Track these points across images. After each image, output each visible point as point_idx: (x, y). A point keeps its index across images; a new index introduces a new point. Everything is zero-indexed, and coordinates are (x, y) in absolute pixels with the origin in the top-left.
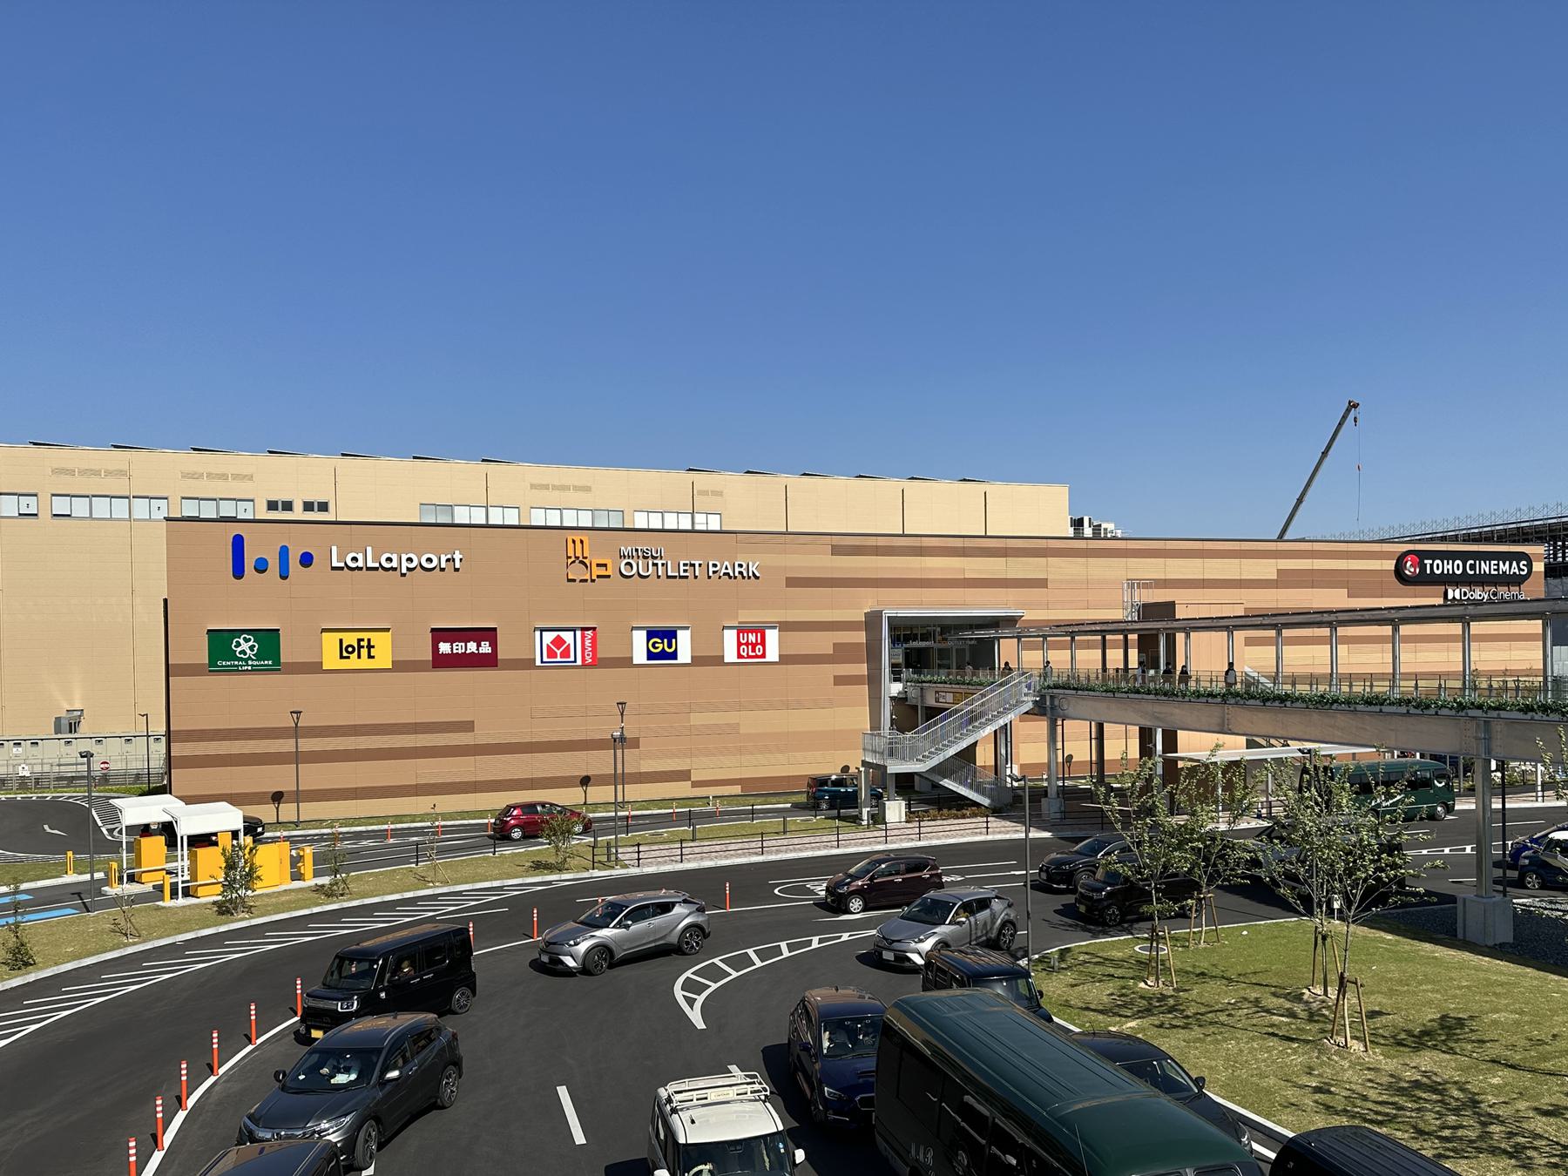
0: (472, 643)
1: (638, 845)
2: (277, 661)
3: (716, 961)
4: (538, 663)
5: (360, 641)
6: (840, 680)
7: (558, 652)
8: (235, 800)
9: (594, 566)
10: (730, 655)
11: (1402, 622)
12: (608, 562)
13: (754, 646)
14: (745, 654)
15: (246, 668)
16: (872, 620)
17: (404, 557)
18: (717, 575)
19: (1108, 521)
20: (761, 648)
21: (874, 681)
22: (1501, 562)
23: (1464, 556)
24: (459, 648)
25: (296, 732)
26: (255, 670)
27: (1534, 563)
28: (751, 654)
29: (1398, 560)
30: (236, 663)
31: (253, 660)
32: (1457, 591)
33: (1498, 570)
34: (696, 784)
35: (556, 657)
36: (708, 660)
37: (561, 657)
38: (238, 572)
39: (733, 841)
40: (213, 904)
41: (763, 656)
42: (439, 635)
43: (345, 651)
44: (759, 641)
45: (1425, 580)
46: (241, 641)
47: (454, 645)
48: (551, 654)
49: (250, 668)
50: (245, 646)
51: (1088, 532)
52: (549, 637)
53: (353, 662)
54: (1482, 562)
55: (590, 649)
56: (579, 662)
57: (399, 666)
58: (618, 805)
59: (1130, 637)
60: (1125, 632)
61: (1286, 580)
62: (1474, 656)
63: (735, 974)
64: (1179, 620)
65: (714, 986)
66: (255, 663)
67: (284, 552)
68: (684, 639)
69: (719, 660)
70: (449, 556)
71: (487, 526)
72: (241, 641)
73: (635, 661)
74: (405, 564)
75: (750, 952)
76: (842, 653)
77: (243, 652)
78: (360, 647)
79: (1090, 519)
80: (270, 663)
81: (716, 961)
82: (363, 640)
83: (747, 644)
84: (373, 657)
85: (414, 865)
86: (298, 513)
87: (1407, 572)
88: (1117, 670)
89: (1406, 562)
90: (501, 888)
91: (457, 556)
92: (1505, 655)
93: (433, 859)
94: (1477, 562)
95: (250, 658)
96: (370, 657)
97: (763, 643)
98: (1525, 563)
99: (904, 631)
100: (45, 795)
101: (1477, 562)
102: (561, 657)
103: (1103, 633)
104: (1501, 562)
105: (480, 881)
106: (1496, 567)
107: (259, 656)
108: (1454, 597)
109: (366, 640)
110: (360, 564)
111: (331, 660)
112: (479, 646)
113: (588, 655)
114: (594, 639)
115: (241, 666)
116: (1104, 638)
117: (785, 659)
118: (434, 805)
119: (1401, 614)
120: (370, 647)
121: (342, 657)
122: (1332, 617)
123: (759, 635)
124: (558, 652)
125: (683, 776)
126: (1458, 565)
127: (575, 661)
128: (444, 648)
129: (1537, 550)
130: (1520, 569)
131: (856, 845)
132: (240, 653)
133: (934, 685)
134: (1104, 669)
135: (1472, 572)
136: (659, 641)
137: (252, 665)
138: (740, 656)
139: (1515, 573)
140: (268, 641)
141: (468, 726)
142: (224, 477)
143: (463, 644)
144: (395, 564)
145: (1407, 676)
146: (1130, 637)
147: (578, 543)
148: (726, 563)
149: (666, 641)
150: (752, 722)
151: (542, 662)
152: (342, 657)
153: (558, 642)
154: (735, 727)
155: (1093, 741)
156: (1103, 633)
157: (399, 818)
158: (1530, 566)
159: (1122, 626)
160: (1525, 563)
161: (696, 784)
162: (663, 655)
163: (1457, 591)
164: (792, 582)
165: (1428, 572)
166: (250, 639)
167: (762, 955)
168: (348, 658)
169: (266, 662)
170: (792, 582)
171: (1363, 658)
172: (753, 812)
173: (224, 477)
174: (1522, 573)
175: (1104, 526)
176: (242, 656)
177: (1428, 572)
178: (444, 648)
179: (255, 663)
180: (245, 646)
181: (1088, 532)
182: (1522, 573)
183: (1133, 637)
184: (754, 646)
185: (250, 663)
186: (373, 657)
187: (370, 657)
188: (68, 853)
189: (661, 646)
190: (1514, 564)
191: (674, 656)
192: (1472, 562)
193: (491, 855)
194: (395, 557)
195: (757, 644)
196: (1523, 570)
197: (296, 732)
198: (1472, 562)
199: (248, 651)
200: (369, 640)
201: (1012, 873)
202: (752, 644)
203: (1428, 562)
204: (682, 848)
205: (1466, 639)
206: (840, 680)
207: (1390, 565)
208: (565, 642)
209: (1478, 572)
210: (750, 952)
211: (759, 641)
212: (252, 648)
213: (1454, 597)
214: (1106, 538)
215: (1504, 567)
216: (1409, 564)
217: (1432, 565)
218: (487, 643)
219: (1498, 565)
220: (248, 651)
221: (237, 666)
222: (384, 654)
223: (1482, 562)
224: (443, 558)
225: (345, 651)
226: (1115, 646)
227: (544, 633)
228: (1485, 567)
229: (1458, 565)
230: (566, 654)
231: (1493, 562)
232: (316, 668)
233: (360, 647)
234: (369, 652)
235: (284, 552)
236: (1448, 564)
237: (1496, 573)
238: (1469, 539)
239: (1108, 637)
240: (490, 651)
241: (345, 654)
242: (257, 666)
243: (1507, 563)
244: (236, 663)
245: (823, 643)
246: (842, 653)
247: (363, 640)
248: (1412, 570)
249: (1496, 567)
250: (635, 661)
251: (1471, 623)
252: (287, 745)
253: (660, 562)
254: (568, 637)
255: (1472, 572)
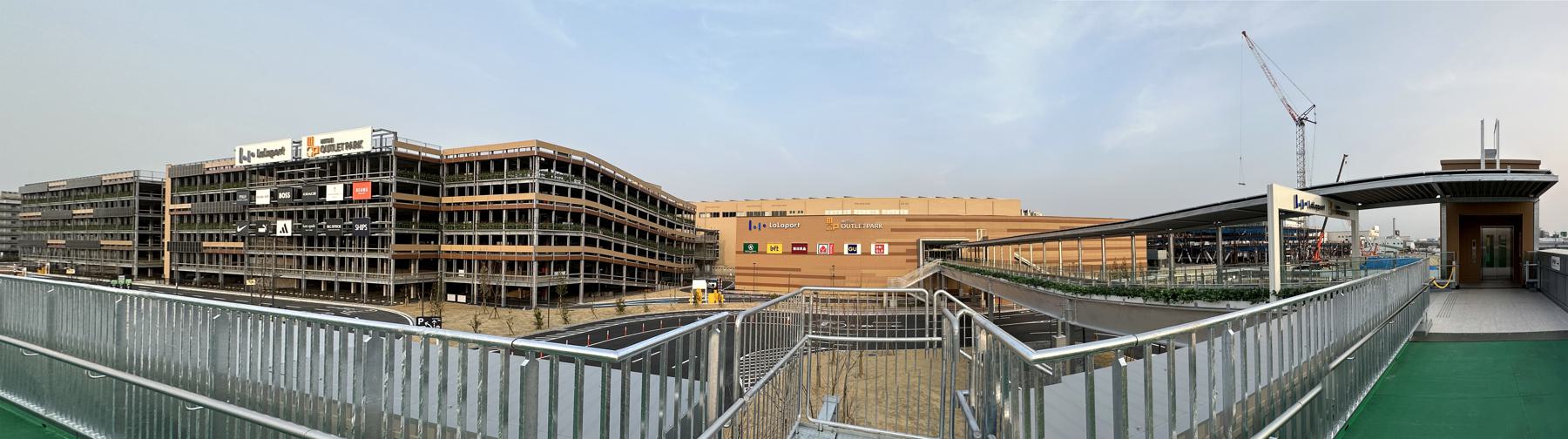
6: (908, 261)
10: (873, 252)
16: (918, 241)
24: (798, 249)
25: (754, 269)
36: (866, 253)
38: (750, 229)
42: (794, 245)
43: (772, 249)
51: (1029, 214)
52: (821, 246)
53: (774, 252)
57: (784, 253)
64: (258, 206)
69: (869, 254)
76: (909, 252)
86: (796, 214)
92: (1093, 254)
99: (928, 245)
111: (769, 251)
117: (890, 254)
128: (795, 249)
140: (756, 246)
142: (780, 206)
153: (823, 248)
164: (893, 230)
170: (893, 230)
171: (1088, 254)
173: (780, 206)
178: (795, 249)
180: (751, 247)
181: (1029, 214)
191: (856, 252)
197: (754, 269)
206: (908, 261)
222: (780, 251)
225: (772, 249)
232: (765, 253)
245: (902, 249)
246: (909, 252)
252: (752, 272)
254: (826, 246)
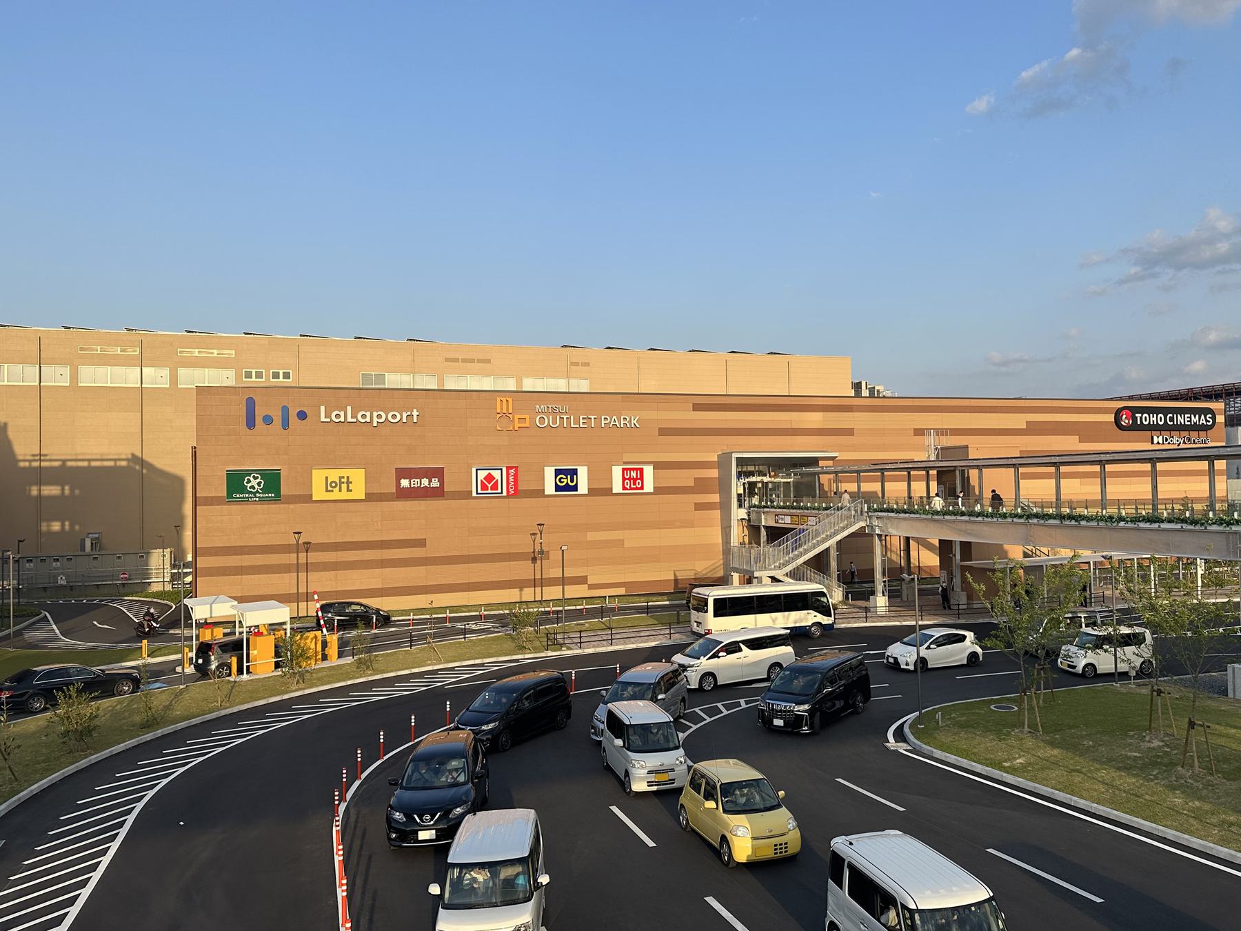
0: (425, 479)
1: (580, 632)
2: (278, 494)
3: (697, 710)
4: (474, 494)
5: (341, 478)
7: (489, 486)
8: (283, 599)
9: (516, 420)
10: (617, 487)
11: (1159, 460)
12: (527, 417)
13: (635, 480)
14: (628, 487)
15: (255, 499)
17: (375, 414)
18: (608, 425)
19: (878, 385)
20: (629, 482)
21: (725, 507)
22: (1192, 416)
23: (1165, 411)
24: (415, 483)
26: (261, 500)
27: (1217, 416)
28: (632, 486)
29: (1116, 414)
30: (247, 495)
31: (260, 493)
32: (1161, 437)
33: (1190, 421)
34: (591, 587)
35: (487, 490)
36: (600, 491)
37: (491, 490)
38: (251, 423)
39: (642, 629)
40: (562, 645)
41: (642, 488)
42: (402, 473)
44: (639, 477)
45: (1136, 427)
46: (251, 479)
47: (412, 481)
48: (484, 487)
49: (257, 499)
50: (254, 483)
54: (1179, 416)
55: (513, 483)
56: (505, 493)
57: (370, 497)
58: (564, 601)
59: (931, 472)
60: (927, 469)
61: (1033, 429)
62: (1109, 488)
63: (709, 720)
65: (695, 727)
66: (261, 495)
67: (285, 410)
68: (583, 473)
69: (608, 491)
70: (409, 413)
71: (789, 396)
72: (251, 479)
73: (547, 493)
74: (375, 420)
75: (719, 705)
77: (253, 487)
78: (341, 483)
79: (866, 383)
80: (273, 495)
81: (697, 710)
82: (343, 477)
83: (630, 479)
84: (351, 491)
85: (409, 648)
87: (1123, 423)
88: (921, 498)
89: (1122, 416)
90: (482, 665)
91: (415, 413)
93: (430, 643)
94: (1175, 415)
95: (257, 492)
96: (349, 490)
97: (642, 478)
98: (1211, 416)
100: (81, 599)
101: (1175, 415)
102: (491, 490)
103: (1056, 465)
104: (1192, 416)
105: (451, 662)
106: (1189, 419)
107: (265, 490)
108: (1158, 437)
109: (346, 477)
110: (342, 419)
111: (319, 493)
112: (430, 481)
113: (512, 488)
114: (516, 476)
115: (251, 498)
116: (909, 473)
117: (658, 490)
118: (432, 602)
119: (1108, 457)
120: (348, 483)
121: (327, 491)
122: (1057, 460)
123: (639, 472)
124: (489, 486)
125: (582, 580)
126: (1161, 418)
127: (502, 493)
128: (405, 483)
129: (1218, 406)
130: (1207, 421)
131: (594, 647)
132: (250, 488)
133: (774, 510)
134: (910, 498)
135: (1172, 423)
136: (564, 477)
137: (259, 497)
138: (624, 488)
139: (1203, 424)
140: (272, 481)
141: (421, 543)
143: (419, 480)
144: (368, 419)
145: (1165, 501)
146: (931, 472)
147: (505, 402)
148: (614, 417)
149: (569, 477)
150: (634, 539)
151: (477, 493)
152: (327, 491)
153: (489, 478)
154: (621, 542)
155: (902, 552)
156: (908, 469)
157: (453, 609)
158: (1214, 418)
159: (1014, 462)
160: (1211, 416)
161: (591, 587)
162: (567, 488)
163: (1161, 437)
164: (664, 432)
165: (1139, 423)
166: (258, 477)
167: (727, 707)
168: (332, 491)
169: (270, 495)
170: (664, 432)
172: (648, 607)
174: (1208, 423)
175: (877, 388)
176: (252, 490)
177: (1139, 423)
178: (405, 483)
179: (261, 495)
180: (254, 483)
181: (865, 393)
182: (1208, 423)
183: (933, 472)
184: (635, 480)
185: (258, 495)
186: (351, 491)
187: (349, 490)
188: (143, 641)
189: (565, 480)
190: (1203, 416)
191: (575, 488)
192: (1171, 415)
193: (463, 640)
194: (368, 414)
195: (637, 479)
196: (1209, 422)
198: (1171, 415)
199: (256, 486)
200: (348, 477)
201: (868, 652)
202: (633, 479)
203: (1138, 415)
204: (612, 634)
205: (1103, 477)
206: (700, 507)
207: (1111, 418)
208: (494, 478)
209: (1175, 423)
210: (719, 705)
211: (639, 477)
212: (249, 481)
213: (1158, 437)
214: (879, 397)
215: (1195, 419)
216: (1124, 416)
217: (1141, 418)
218: (437, 479)
219: (1190, 417)
220: (256, 486)
221: (248, 498)
223: (1179, 416)
224: (405, 415)
226: (918, 479)
227: (478, 471)
228: (1180, 419)
229: (1161, 418)
230: (495, 487)
231: (1186, 416)
233: (341, 483)
234: (348, 487)
235: (285, 410)
236: (1153, 417)
237: (1189, 423)
238: (1151, 397)
239: (912, 473)
240: (438, 486)
241: (329, 488)
242: (263, 497)
243: (1197, 416)
244: (247, 495)
245: (686, 478)
246: (701, 486)
247: (343, 477)
248: (1127, 421)
249: (1189, 419)
250: (547, 493)
251: (1215, 461)
253: (565, 417)
254: (497, 474)
255: (1172, 423)
